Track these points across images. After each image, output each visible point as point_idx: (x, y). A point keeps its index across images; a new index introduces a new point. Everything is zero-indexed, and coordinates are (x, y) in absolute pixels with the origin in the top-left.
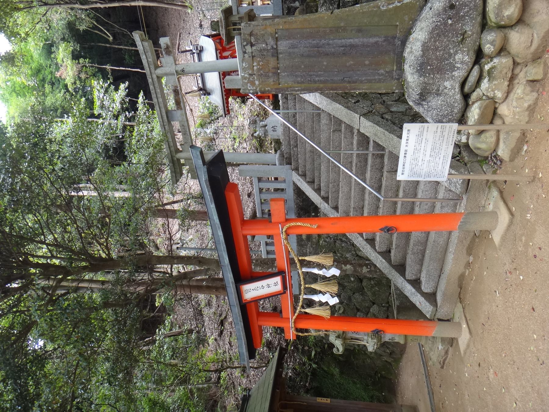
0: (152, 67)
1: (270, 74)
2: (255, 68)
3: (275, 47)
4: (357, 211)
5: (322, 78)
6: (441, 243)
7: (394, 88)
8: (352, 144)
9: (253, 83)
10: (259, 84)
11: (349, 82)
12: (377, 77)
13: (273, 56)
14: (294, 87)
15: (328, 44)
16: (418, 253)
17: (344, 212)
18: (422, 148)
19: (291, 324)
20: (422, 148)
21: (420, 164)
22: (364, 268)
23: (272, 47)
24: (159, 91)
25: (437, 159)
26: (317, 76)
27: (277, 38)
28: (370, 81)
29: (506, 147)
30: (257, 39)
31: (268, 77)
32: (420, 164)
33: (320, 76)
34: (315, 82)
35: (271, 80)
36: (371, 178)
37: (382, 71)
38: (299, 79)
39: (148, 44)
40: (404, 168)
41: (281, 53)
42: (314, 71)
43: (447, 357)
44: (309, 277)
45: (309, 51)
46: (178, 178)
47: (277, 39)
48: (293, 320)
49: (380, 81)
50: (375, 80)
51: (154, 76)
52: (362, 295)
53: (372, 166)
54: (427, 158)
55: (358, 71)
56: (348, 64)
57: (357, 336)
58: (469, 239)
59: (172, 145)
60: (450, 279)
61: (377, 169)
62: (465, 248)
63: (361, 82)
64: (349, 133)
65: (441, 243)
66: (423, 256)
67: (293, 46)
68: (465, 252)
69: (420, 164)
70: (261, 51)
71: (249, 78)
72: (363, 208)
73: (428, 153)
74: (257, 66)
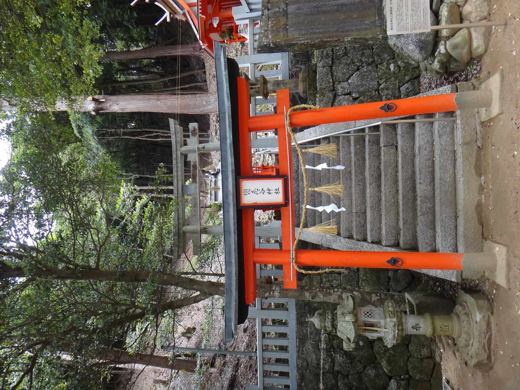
0: (179, 145)
1: (281, 30)
2: (270, 26)
3: (285, 9)
4: (359, 216)
5: (321, 30)
6: (448, 180)
7: (379, 33)
8: (350, 153)
9: (267, 37)
10: (272, 38)
11: (342, 32)
12: (364, 27)
13: (284, 16)
14: (299, 38)
15: (325, 5)
16: (427, 213)
17: (347, 230)
18: (404, 4)
19: (293, 254)
20: (404, 4)
21: (405, 18)
22: (373, 295)
23: (283, 9)
24: (180, 165)
25: (419, 13)
26: (317, 29)
27: (287, 4)
28: (358, 30)
29: (478, 34)
30: (272, 6)
31: (279, 32)
32: (405, 18)
33: (320, 28)
34: (315, 33)
35: (281, 34)
36: (370, 166)
37: (367, 22)
38: (303, 32)
39: (180, 128)
40: (392, 24)
41: (290, 14)
42: (315, 25)
43: (491, 335)
44: (310, 372)
45: (311, 11)
46: (180, 253)
47: (287, 4)
48: (294, 247)
49: (366, 29)
50: (363, 29)
51: (179, 153)
52: (374, 368)
53: (369, 154)
54: (410, 12)
55: (349, 22)
56: (341, 18)
57: (372, 320)
58: (474, 154)
59: (181, 217)
60: (467, 213)
61: (374, 156)
62: (473, 166)
63: (352, 31)
64: (347, 143)
65: (448, 180)
66: (434, 216)
67: (299, 9)
68: (474, 172)
69: (405, 18)
70: (275, 13)
71: (264, 33)
72: (365, 213)
73: (410, 8)
74: (271, 24)
